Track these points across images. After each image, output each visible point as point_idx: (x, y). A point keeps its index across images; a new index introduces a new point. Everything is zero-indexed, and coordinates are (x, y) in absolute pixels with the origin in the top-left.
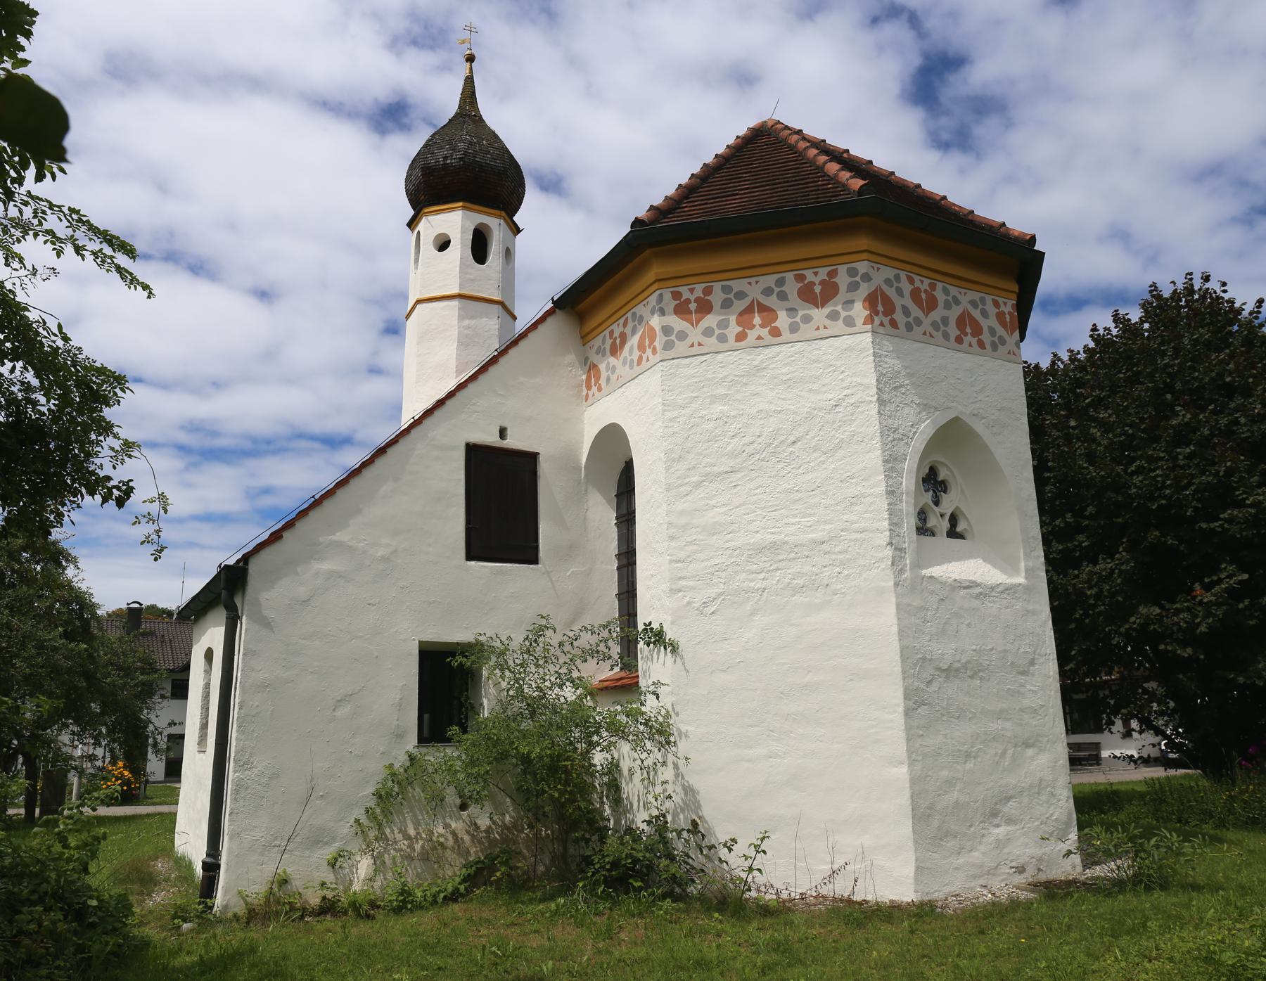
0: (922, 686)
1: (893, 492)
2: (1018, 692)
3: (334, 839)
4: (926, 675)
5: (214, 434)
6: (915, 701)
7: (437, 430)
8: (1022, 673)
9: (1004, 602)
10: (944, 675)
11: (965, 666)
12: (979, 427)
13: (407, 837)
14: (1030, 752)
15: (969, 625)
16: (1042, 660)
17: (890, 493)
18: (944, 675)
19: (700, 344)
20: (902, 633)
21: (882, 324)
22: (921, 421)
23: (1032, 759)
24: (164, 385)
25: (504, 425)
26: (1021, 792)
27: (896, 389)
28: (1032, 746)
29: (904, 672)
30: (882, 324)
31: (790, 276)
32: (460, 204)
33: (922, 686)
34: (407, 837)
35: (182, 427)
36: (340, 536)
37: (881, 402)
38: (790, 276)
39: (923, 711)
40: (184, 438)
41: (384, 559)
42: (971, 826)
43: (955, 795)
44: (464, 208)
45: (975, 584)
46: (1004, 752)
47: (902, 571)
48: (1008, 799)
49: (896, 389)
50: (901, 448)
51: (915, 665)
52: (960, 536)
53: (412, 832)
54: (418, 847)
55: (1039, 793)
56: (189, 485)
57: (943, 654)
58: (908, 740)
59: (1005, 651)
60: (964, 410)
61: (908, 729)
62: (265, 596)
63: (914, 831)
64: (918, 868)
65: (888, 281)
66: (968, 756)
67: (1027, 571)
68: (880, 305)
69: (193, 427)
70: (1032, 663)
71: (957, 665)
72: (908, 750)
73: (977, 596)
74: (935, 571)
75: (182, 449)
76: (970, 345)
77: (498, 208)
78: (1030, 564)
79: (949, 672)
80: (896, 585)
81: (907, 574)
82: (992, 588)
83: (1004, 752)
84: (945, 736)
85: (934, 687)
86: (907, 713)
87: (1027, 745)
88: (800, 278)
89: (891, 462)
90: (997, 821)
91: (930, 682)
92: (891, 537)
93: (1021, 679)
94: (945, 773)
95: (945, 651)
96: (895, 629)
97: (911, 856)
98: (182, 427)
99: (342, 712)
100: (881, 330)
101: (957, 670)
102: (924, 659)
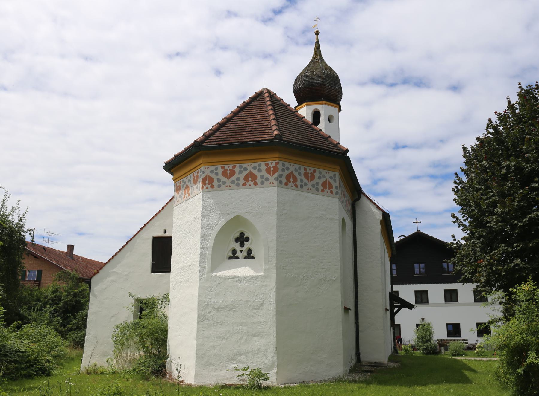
0: (206, 314)
1: (203, 248)
2: (252, 316)
3: (109, 355)
4: (208, 310)
5: (446, 166)
6: (201, 319)
7: (143, 234)
8: (256, 309)
9: (250, 283)
10: (216, 310)
11: (227, 307)
12: (248, 217)
13: (127, 356)
14: (255, 338)
15: (231, 292)
16: (267, 304)
17: (202, 248)
18: (216, 310)
19: (230, 186)
20: (199, 296)
21: (207, 188)
22: (220, 220)
23: (256, 341)
24: (417, 146)
25: (166, 228)
26: (248, 353)
27: (210, 210)
28: (257, 336)
29: (198, 309)
30: (207, 188)
31: (219, 167)
32: (305, 104)
33: (206, 314)
34: (127, 356)
35: (430, 166)
36: (115, 270)
37: (203, 216)
38: (219, 167)
39: (206, 322)
40: (432, 171)
41: (127, 275)
42: (221, 362)
43: (216, 351)
44: (307, 105)
45: (237, 277)
46: (242, 338)
47: (203, 275)
48: (241, 355)
49: (210, 210)
50: (209, 231)
51: (204, 307)
52: (253, 258)
53: (129, 354)
54: (129, 359)
55: (257, 354)
56: (440, 195)
57: (216, 303)
58: (198, 332)
59: (247, 301)
60: (241, 212)
61: (198, 328)
62: (95, 288)
63: (196, 362)
64: (196, 374)
65: (212, 172)
66: (224, 338)
67: (264, 270)
68: (208, 182)
69: (436, 165)
70: (262, 305)
71: (222, 306)
72: (197, 335)
73: (237, 281)
74: (218, 274)
75: (433, 177)
76: (250, 185)
77: (321, 100)
78: (267, 267)
79: (218, 309)
80: (200, 280)
81: (205, 276)
82: (245, 278)
83: (242, 338)
84: (214, 331)
85: (212, 314)
86: (198, 323)
87: (254, 335)
88: (223, 168)
89: (204, 237)
90: (235, 362)
91: (210, 312)
92: (200, 263)
93: (255, 311)
94: (212, 344)
95: (218, 301)
96: (197, 295)
97: (194, 369)
98: (430, 166)
99: (113, 320)
100: (207, 190)
101: (222, 308)
102: (208, 305)
